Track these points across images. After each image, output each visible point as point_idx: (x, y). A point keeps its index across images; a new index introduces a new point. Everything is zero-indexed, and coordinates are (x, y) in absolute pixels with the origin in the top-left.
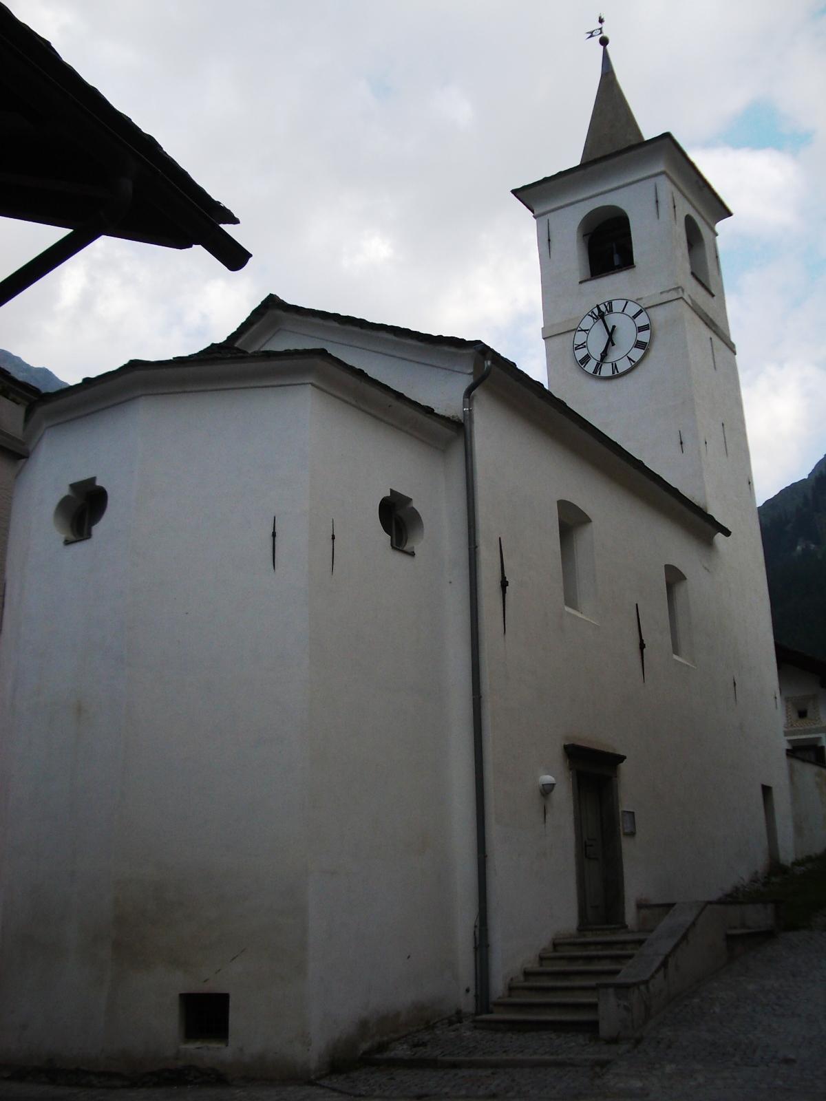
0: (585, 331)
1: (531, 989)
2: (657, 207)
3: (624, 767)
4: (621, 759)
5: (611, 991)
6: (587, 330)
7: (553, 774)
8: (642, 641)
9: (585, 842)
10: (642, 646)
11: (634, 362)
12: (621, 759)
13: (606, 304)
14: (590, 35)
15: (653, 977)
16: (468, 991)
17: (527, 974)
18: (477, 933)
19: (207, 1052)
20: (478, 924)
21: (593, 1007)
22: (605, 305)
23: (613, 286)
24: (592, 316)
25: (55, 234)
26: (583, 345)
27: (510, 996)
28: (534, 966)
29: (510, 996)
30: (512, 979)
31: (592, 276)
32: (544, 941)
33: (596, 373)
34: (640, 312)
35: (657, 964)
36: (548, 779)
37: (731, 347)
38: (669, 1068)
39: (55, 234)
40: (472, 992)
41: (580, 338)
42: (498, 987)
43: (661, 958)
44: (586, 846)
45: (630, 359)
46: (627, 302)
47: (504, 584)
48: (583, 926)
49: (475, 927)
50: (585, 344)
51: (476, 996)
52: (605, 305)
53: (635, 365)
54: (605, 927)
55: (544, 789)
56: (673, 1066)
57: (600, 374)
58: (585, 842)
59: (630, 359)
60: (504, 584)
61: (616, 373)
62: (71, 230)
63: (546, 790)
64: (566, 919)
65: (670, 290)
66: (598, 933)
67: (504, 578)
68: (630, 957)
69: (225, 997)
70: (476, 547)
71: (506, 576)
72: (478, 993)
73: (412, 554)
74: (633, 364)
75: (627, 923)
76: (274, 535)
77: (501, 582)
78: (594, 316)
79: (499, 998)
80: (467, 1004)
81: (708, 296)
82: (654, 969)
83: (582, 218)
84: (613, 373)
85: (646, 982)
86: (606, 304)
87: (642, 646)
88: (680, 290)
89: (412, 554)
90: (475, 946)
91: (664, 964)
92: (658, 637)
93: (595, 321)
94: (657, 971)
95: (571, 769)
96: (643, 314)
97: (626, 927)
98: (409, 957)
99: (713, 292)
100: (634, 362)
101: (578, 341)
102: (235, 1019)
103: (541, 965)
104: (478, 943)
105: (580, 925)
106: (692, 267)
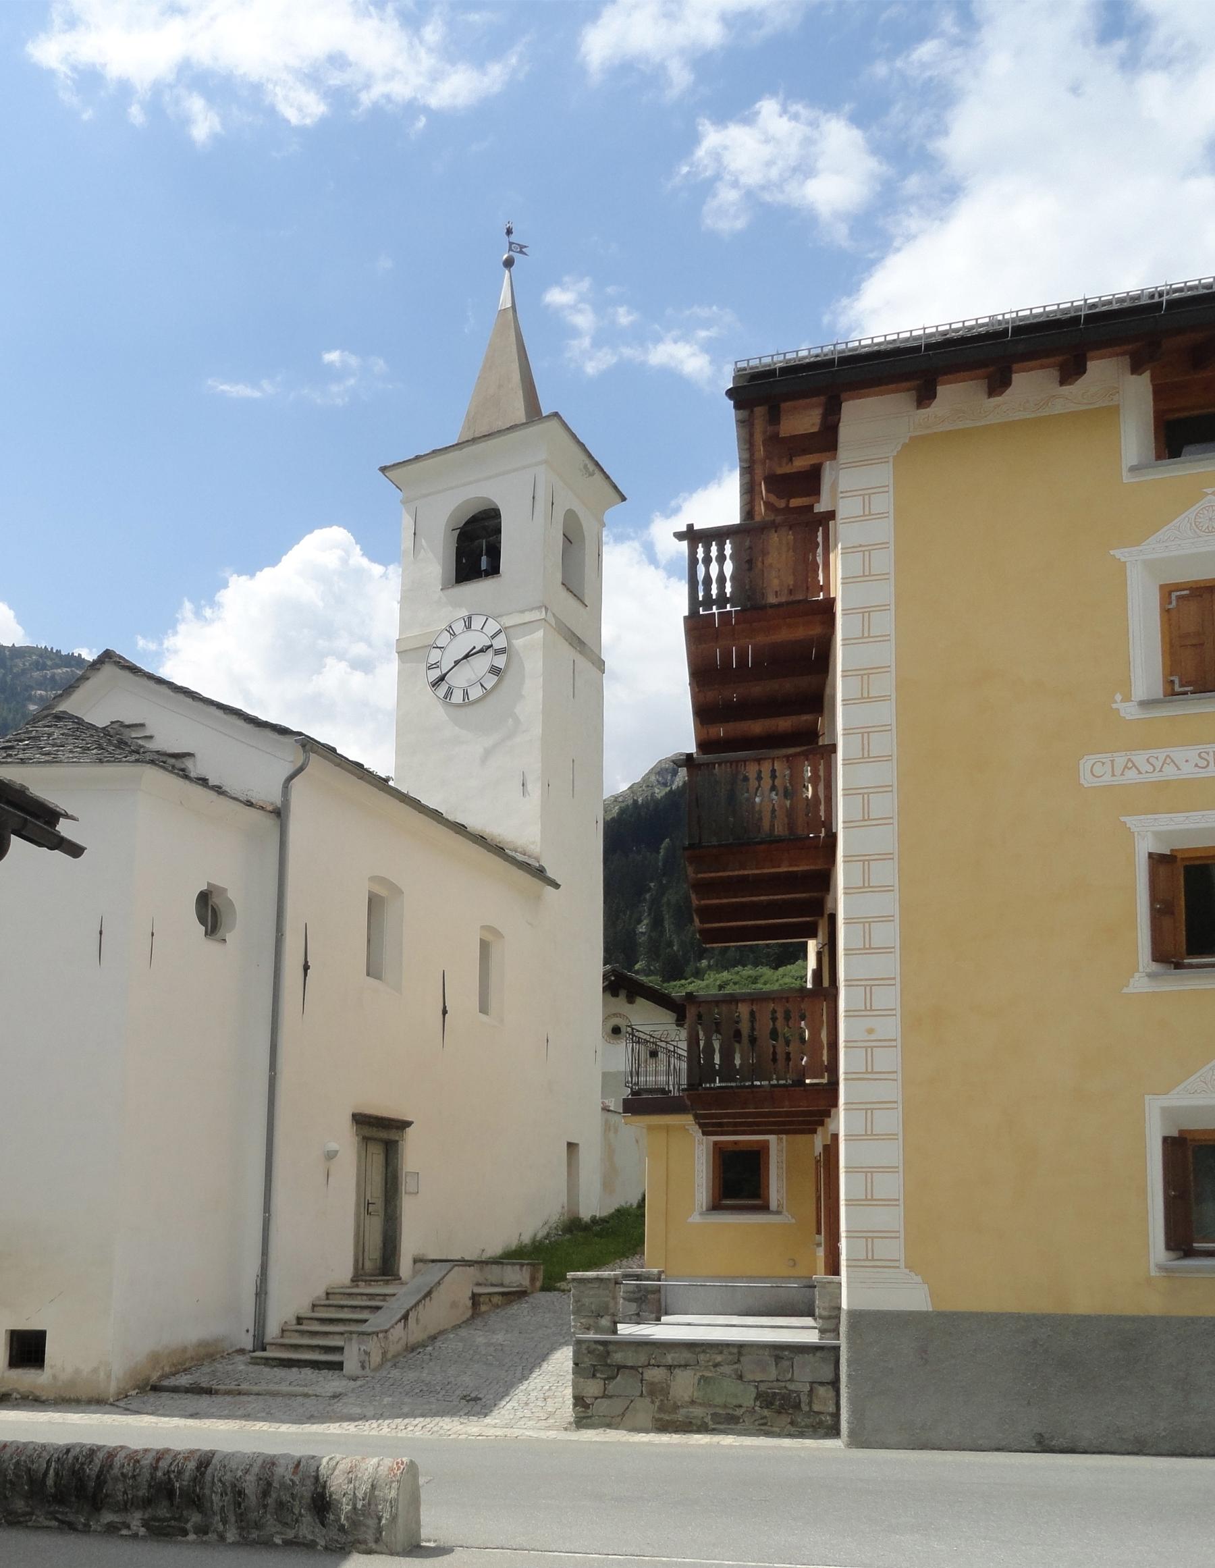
0: (440, 648)
1: (302, 1333)
3: (409, 1130)
4: (409, 1124)
5: (355, 1336)
6: (443, 648)
7: (345, 1141)
8: (445, 1007)
9: (368, 1200)
10: (445, 1012)
11: (486, 689)
12: (409, 1124)
13: (466, 619)
15: (392, 1327)
16: (248, 1331)
17: (299, 1320)
19: (26, 1378)
20: (259, 1274)
21: (340, 1349)
22: (464, 619)
24: (449, 632)
27: (282, 1337)
28: (305, 1311)
29: (282, 1337)
30: (286, 1322)
32: (320, 1291)
33: (446, 698)
34: (500, 631)
35: (399, 1316)
36: (333, 1146)
37: (600, 665)
38: (387, 1400)
41: (435, 656)
42: (272, 1330)
43: (403, 1312)
44: (368, 1204)
45: (482, 685)
46: (487, 619)
48: (355, 1279)
49: (258, 1276)
50: (439, 664)
51: (254, 1336)
52: (464, 619)
53: (488, 693)
54: (380, 1278)
55: (328, 1155)
56: (390, 1399)
57: (450, 700)
58: (368, 1200)
63: (330, 1156)
64: (340, 1271)
66: (373, 1283)
68: (378, 1308)
70: (282, 935)
71: (308, 960)
72: (256, 1333)
74: (485, 691)
75: (401, 1275)
76: (101, 933)
77: (304, 966)
78: (434, 666)
79: (273, 1338)
80: (247, 1342)
81: (581, 607)
82: (394, 1321)
83: (453, 508)
84: (464, 700)
85: (386, 1331)
86: (466, 619)
87: (445, 1012)
88: (543, 609)
90: (1171, 640)
91: (405, 1317)
92: (463, 999)
93: (452, 637)
94: (400, 1321)
95: (357, 1135)
96: (502, 635)
97: (400, 1279)
98: (197, 1301)
99: (586, 603)
100: (486, 689)
103: (313, 1311)
104: (258, 1290)
105: (354, 1277)
106: (563, 579)
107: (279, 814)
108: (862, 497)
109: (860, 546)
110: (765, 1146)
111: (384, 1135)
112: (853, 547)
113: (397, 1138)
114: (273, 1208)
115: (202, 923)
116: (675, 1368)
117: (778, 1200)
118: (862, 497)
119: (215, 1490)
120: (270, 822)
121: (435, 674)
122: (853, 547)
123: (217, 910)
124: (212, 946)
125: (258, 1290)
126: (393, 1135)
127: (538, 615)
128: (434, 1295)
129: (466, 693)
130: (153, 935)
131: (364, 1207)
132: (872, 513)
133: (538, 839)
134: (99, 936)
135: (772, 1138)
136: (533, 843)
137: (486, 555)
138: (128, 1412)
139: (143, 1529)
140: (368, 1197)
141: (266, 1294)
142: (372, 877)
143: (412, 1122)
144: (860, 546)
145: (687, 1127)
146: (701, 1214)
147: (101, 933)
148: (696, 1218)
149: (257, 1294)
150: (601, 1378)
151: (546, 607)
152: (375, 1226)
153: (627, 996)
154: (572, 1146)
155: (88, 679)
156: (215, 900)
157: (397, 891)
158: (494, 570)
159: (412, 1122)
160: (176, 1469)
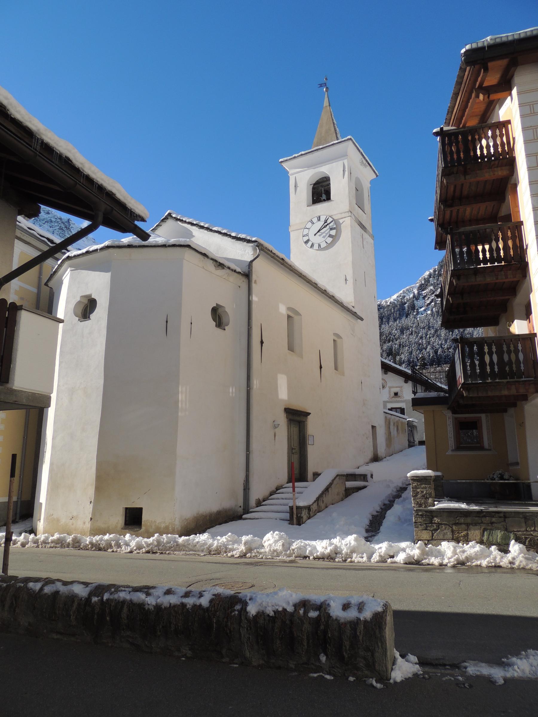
2: (262, 346)
3: (309, 417)
4: (309, 414)
7: (282, 419)
8: (321, 365)
10: (321, 367)
12: (309, 414)
14: (320, 86)
18: (245, 484)
20: (245, 480)
23: (322, 208)
25: (86, 224)
26: (307, 235)
31: (313, 204)
39: (86, 224)
40: (242, 507)
45: (326, 242)
47: (262, 342)
49: (244, 481)
59: (326, 242)
60: (262, 342)
61: (320, 248)
62: (91, 223)
65: (345, 212)
67: (262, 340)
69: (142, 508)
70: (251, 328)
73: (225, 329)
76: (167, 322)
84: (319, 248)
87: (321, 367)
89: (225, 329)
95: (287, 418)
101: (305, 233)
102: (145, 517)
104: (245, 488)
107: (247, 275)
108: (529, 106)
109: (531, 127)
110: (480, 419)
111: (298, 418)
112: (528, 127)
113: (304, 420)
114: (251, 449)
115: (214, 320)
116: (470, 525)
117: (489, 444)
118: (529, 106)
119: (243, 625)
120: (242, 282)
121: (306, 239)
122: (528, 127)
123: (220, 316)
124: (219, 330)
125: (245, 488)
126: (302, 418)
127: (347, 214)
128: (330, 490)
129: (319, 245)
130: (191, 323)
131: (291, 450)
132: (535, 112)
133: (353, 300)
134: (166, 323)
135: (483, 416)
136: (351, 302)
137: (325, 194)
138: (221, 261)
139: (190, 652)
140: (292, 446)
141: (249, 489)
142: (288, 307)
143: (310, 413)
144: (531, 127)
145: (442, 411)
146: (452, 451)
147: (167, 322)
148: (449, 453)
149: (244, 490)
150: (430, 530)
151: (351, 212)
152: (296, 458)
153: (384, 371)
154: (373, 427)
155: (161, 226)
156: (220, 311)
157: (297, 313)
158: (328, 198)
159: (310, 413)
160: (213, 609)
